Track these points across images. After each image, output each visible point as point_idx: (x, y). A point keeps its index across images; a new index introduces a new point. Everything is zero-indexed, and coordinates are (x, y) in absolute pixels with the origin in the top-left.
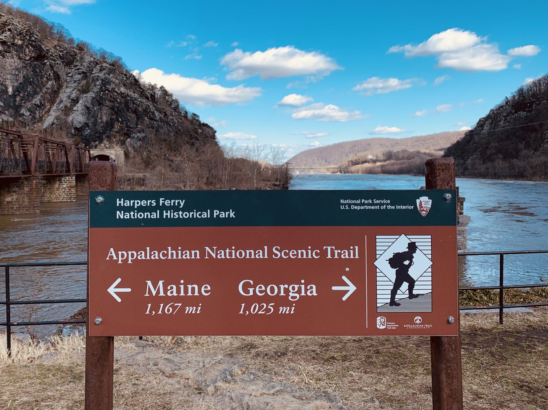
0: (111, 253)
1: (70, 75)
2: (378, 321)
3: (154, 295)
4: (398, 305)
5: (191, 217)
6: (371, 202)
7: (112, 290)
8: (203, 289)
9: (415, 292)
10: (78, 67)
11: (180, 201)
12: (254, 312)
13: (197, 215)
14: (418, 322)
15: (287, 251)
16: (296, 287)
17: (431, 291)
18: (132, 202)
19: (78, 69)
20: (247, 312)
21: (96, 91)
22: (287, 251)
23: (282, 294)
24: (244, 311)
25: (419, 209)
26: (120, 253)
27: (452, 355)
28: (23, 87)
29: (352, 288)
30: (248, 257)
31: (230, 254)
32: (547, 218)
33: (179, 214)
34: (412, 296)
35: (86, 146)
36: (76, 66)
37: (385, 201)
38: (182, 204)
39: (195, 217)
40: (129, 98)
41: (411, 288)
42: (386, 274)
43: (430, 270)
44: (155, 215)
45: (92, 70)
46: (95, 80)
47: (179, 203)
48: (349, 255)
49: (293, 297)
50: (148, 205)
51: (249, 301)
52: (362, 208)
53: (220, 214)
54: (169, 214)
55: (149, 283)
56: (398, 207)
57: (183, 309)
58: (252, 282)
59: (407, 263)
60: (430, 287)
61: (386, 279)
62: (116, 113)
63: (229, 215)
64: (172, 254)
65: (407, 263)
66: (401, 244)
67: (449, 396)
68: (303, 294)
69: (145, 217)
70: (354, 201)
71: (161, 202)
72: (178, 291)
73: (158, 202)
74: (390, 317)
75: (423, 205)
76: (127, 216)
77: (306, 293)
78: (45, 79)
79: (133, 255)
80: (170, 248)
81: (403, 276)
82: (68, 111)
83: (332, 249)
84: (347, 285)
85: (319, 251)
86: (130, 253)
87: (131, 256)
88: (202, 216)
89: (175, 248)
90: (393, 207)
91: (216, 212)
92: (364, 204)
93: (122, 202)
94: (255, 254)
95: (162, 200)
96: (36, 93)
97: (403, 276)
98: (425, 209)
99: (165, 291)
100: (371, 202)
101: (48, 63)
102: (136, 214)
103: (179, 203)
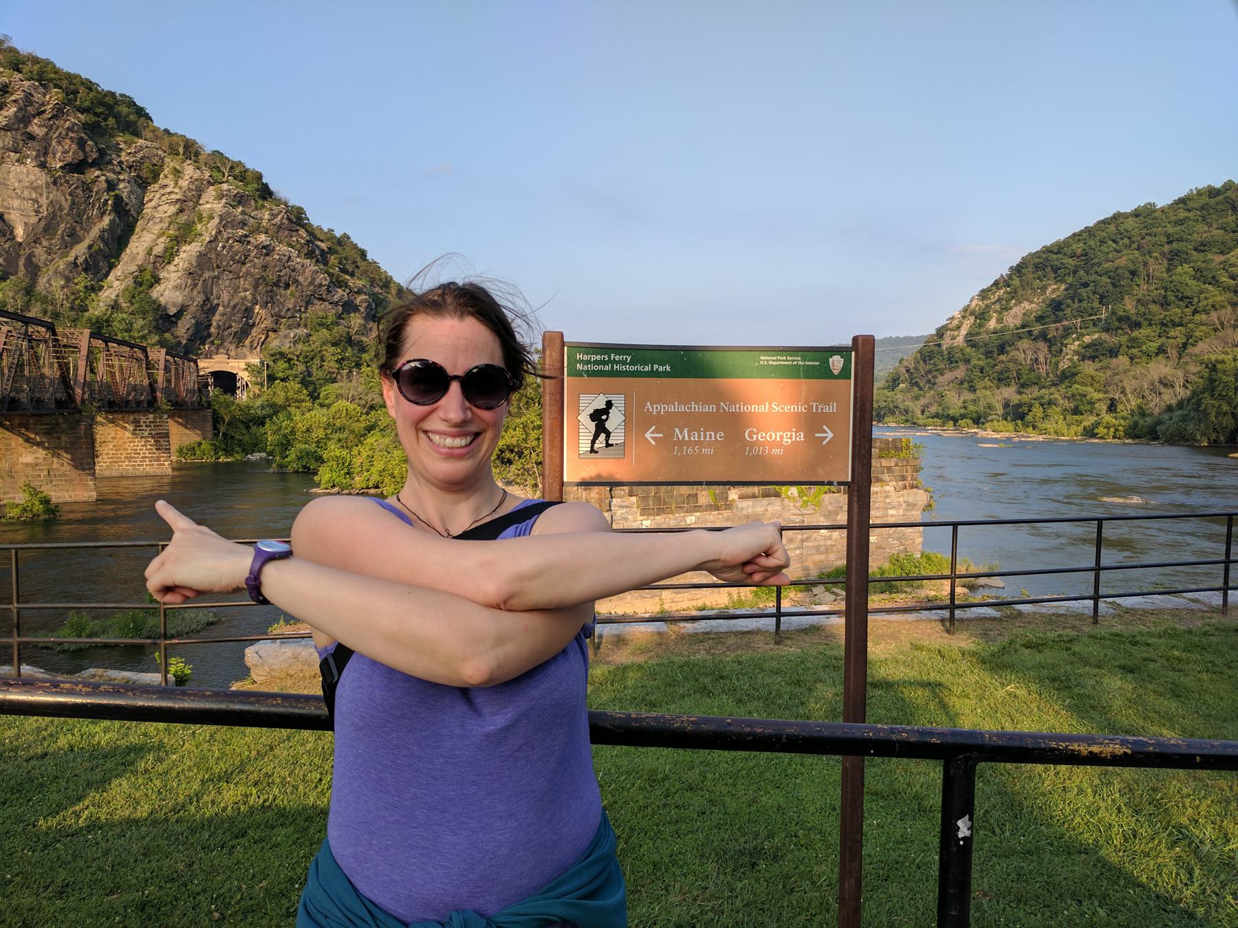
10: (168, 190)
34: (608, 445)
44: (607, 368)
59: (604, 417)
65: (604, 417)
72: (699, 436)
87: (662, 408)
97: (601, 429)
99: (689, 436)
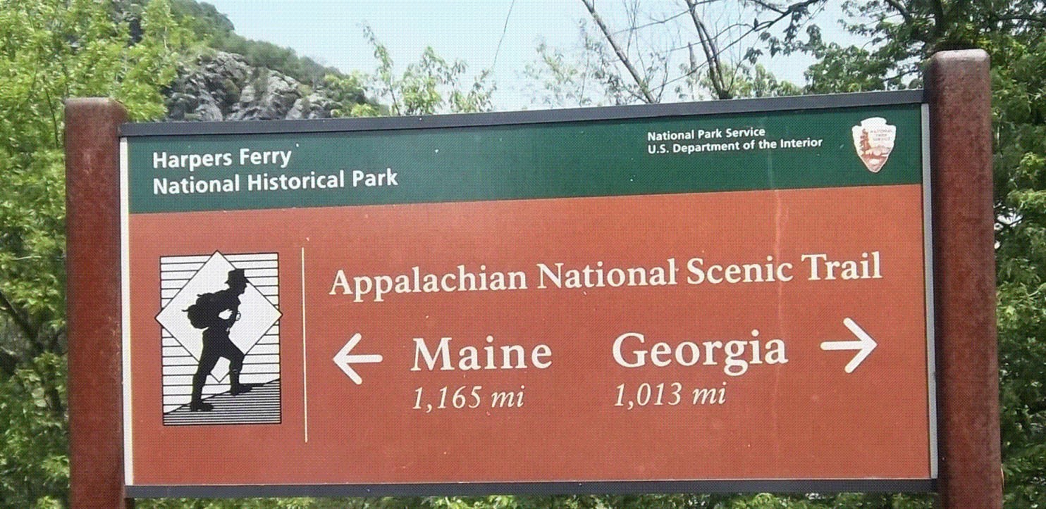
0: (340, 281)
3: (431, 368)
4: (209, 408)
5: (305, 187)
6: (719, 135)
7: (865, 345)
8: (535, 355)
9: (243, 380)
11: (282, 153)
12: (643, 401)
13: (317, 182)
15: (720, 268)
16: (741, 345)
17: (277, 376)
18: (184, 158)
20: (631, 403)
22: (720, 268)
23: (709, 361)
25: (860, 153)
26: (358, 280)
30: (632, 283)
31: (594, 278)
33: (279, 182)
37: (753, 133)
38: (286, 160)
39: (313, 186)
41: (235, 371)
43: (276, 330)
47: (279, 157)
48: (860, 272)
49: (733, 369)
50: (217, 164)
51: (633, 378)
52: (699, 149)
53: (365, 179)
54: (259, 182)
55: (420, 344)
56: (784, 144)
58: (641, 337)
59: (225, 315)
60: (277, 368)
61: (182, 352)
63: (385, 180)
64: (467, 281)
65: (225, 315)
69: (212, 190)
70: (680, 135)
71: (243, 157)
72: (482, 359)
73: (236, 157)
75: (871, 142)
76: (175, 189)
77: (762, 357)
80: (462, 268)
81: (218, 344)
83: (819, 260)
84: (855, 338)
85: (790, 266)
86: (378, 279)
88: (329, 184)
90: (773, 145)
91: (358, 176)
92: (704, 141)
93: (164, 160)
94: (648, 277)
95: (246, 153)
97: (218, 344)
98: (877, 153)
99: (455, 359)
100: (719, 135)
102: (192, 183)
103: (279, 157)
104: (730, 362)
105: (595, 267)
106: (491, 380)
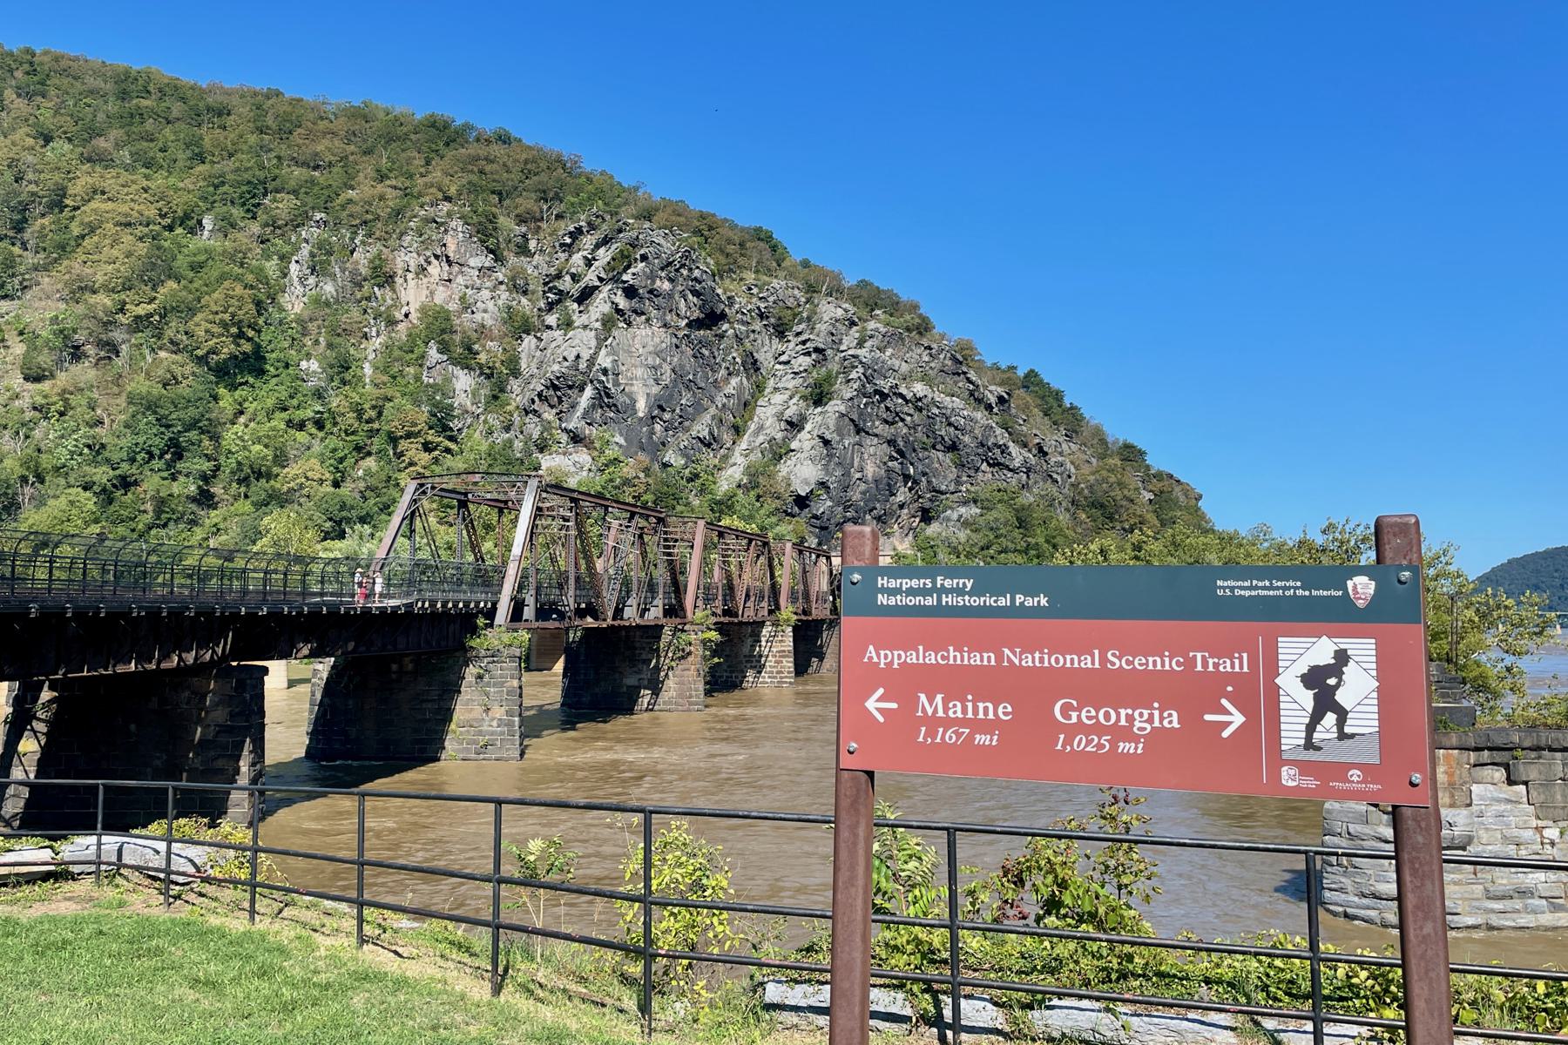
1: (783, 358)
2: (1284, 774)
4: (1319, 749)
7: (872, 704)
8: (1000, 710)
9: (1347, 730)
13: (990, 601)
14: (1355, 779)
16: (1146, 713)
19: (804, 343)
21: (849, 395)
23: (1123, 722)
24: (1064, 746)
27: (1420, 839)
28: (671, 396)
29: (1238, 719)
32: (3, 303)
34: (1342, 736)
35: (820, 544)
36: (798, 334)
37: (1291, 583)
38: (969, 585)
40: (936, 411)
41: (1341, 723)
42: (1297, 700)
43: (1375, 695)
45: (841, 342)
46: (849, 363)
48: (1233, 666)
55: (923, 697)
56: (1314, 593)
57: (971, 737)
59: (1332, 681)
61: (1295, 706)
62: (901, 453)
65: (1332, 681)
66: (1322, 651)
67: (1417, 907)
68: (1157, 724)
72: (964, 711)
73: (934, 582)
74: (1304, 768)
76: (892, 602)
78: (723, 372)
79: (899, 657)
81: (1326, 702)
82: (778, 452)
83: (1203, 657)
87: (897, 657)
89: (959, 649)
92: (1257, 588)
96: (699, 409)
97: (1326, 702)
99: (946, 709)
101: (731, 332)
104: (1137, 724)
105: (1042, 652)
106: (979, 726)
